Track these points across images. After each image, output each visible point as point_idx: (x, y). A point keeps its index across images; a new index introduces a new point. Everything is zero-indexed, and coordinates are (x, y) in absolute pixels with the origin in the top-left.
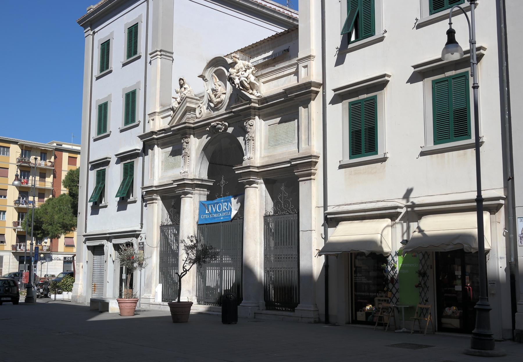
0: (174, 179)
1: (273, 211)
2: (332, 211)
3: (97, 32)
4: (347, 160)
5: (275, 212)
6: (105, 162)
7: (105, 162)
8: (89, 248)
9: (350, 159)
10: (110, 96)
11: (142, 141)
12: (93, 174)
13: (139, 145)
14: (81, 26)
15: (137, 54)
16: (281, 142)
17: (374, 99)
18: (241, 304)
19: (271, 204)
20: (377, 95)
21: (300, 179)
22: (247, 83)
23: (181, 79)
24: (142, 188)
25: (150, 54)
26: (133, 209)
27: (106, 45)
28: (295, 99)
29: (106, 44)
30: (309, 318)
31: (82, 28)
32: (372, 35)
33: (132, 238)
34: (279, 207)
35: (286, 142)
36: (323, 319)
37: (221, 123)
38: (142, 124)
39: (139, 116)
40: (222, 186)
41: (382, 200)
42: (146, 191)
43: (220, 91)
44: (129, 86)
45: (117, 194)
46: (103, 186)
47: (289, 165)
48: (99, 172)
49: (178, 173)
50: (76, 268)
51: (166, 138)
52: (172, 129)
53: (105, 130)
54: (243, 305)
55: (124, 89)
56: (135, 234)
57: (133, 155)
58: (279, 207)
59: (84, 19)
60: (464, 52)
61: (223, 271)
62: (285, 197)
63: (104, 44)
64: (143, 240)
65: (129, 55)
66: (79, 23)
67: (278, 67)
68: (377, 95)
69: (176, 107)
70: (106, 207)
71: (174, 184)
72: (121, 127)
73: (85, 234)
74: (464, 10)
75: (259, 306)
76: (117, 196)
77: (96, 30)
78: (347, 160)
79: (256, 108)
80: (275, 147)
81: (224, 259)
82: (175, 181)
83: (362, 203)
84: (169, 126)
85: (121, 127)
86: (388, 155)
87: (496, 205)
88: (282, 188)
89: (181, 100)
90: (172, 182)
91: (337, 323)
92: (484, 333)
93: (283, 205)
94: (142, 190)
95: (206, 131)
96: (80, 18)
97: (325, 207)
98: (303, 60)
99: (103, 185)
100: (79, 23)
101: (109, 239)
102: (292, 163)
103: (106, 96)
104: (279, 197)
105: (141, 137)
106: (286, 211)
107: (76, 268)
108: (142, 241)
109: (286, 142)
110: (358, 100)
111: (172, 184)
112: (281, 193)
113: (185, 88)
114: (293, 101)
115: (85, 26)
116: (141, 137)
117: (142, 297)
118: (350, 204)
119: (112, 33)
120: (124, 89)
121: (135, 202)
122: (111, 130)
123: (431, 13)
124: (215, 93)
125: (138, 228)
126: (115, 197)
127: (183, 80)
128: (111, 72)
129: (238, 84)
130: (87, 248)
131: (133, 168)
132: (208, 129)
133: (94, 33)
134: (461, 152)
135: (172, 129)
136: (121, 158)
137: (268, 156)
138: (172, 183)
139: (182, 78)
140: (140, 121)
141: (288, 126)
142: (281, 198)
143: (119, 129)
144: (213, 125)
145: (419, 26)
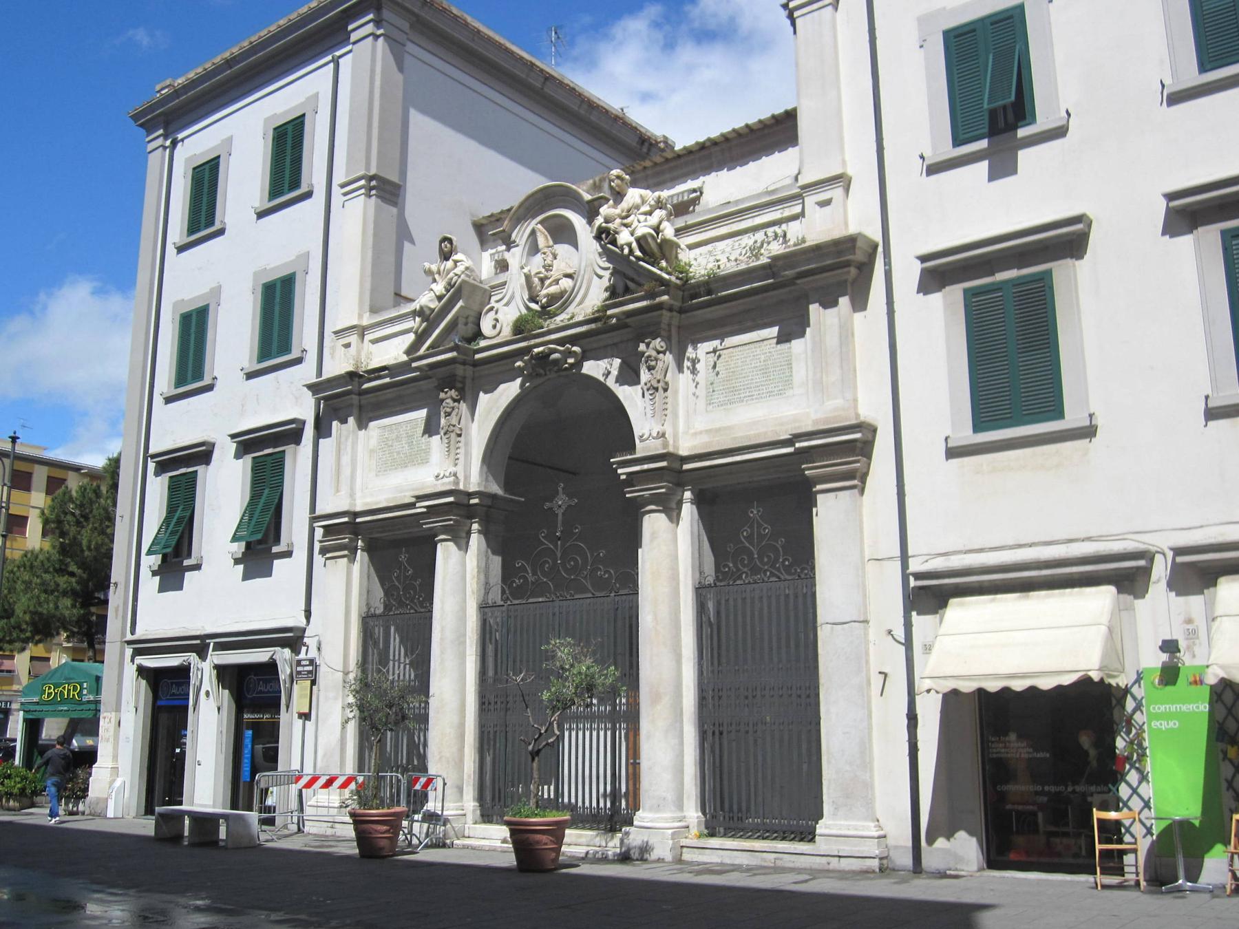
0: (421, 493)
1: (382, 606)
3: (182, 140)
4: (966, 435)
5: (387, 607)
6: (202, 454)
7: (202, 454)
8: (142, 671)
10: (217, 291)
12: (158, 488)
13: (305, 409)
14: (141, 126)
16: (748, 394)
19: (379, 593)
21: (819, 487)
23: (445, 239)
25: (343, 186)
26: (290, 572)
29: (207, 167)
31: (142, 131)
33: (189, 654)
34: (746, 562)
38: (311, 358)
39: (305, 334)
40: (560, 512)
41: (1083, 536)
42: (323, 527)
43: (557, 270)
44: (275, 262)
45: (236, 531)
46: (188, 514)
47: (790, 450)
51: (388, 391)
52: (414, 365)
53: (198, 374)
56: (292, 639)
57: (290, 434)
58: (746, 562)
59: (151, 109)
61: (567, 734)
62: (761, 537)
63: (202, 168)
64: (313, 653)
66: (135, 118)
69: (430, 309)
70: (197, 567)
71: (418, 505)
72: (247, 366)
73: (129, 637)
75: (688, 827)
76: (235, 539)
77: (180, 136)
78: (966, 435)
80: (729, 406)
82: (420, 498)
83: (1020, 546)
84: (405, 358)
86: (1099, 421)
87: (1134, 570)
88: (752, 512)
89: (448, 291)
90: (413, 500)
92: (224, 746)
93: (756, 556)
95: (514, 369)
96: (139, 105)
97: (904, 557)
99: (190, 511)
100: (135, 118)
101: (202, 652)
102: (797, 445)
104: (744, 537)
106: (768, 573)
108: (310, 656)
110: (993, 284)
111: (412, 505)
112: (751, 527)
113: (456, 262)
114: (793, 288)
115: (149, 127)
117: (308, 804)
118: (981, 550)
119: (230, 140)
120: (256, 275)
121: (288, 554)
122: (216, 374)
124: (542, 275)
125: (301, 622)
126: (231, 542)
127: (450, 241)
128: (221, 232)
129: (629, 245)
130: (1169, 688)
132: (519, 364)
133: (174, 143)
135: (414, 365)
136: (247, 443)
137: (708, 431)
139: (449, 236)
141: (770, 352)
142: (749, 538)
143: (242, 370)
144: (539, 353)
145: (1175, 99)
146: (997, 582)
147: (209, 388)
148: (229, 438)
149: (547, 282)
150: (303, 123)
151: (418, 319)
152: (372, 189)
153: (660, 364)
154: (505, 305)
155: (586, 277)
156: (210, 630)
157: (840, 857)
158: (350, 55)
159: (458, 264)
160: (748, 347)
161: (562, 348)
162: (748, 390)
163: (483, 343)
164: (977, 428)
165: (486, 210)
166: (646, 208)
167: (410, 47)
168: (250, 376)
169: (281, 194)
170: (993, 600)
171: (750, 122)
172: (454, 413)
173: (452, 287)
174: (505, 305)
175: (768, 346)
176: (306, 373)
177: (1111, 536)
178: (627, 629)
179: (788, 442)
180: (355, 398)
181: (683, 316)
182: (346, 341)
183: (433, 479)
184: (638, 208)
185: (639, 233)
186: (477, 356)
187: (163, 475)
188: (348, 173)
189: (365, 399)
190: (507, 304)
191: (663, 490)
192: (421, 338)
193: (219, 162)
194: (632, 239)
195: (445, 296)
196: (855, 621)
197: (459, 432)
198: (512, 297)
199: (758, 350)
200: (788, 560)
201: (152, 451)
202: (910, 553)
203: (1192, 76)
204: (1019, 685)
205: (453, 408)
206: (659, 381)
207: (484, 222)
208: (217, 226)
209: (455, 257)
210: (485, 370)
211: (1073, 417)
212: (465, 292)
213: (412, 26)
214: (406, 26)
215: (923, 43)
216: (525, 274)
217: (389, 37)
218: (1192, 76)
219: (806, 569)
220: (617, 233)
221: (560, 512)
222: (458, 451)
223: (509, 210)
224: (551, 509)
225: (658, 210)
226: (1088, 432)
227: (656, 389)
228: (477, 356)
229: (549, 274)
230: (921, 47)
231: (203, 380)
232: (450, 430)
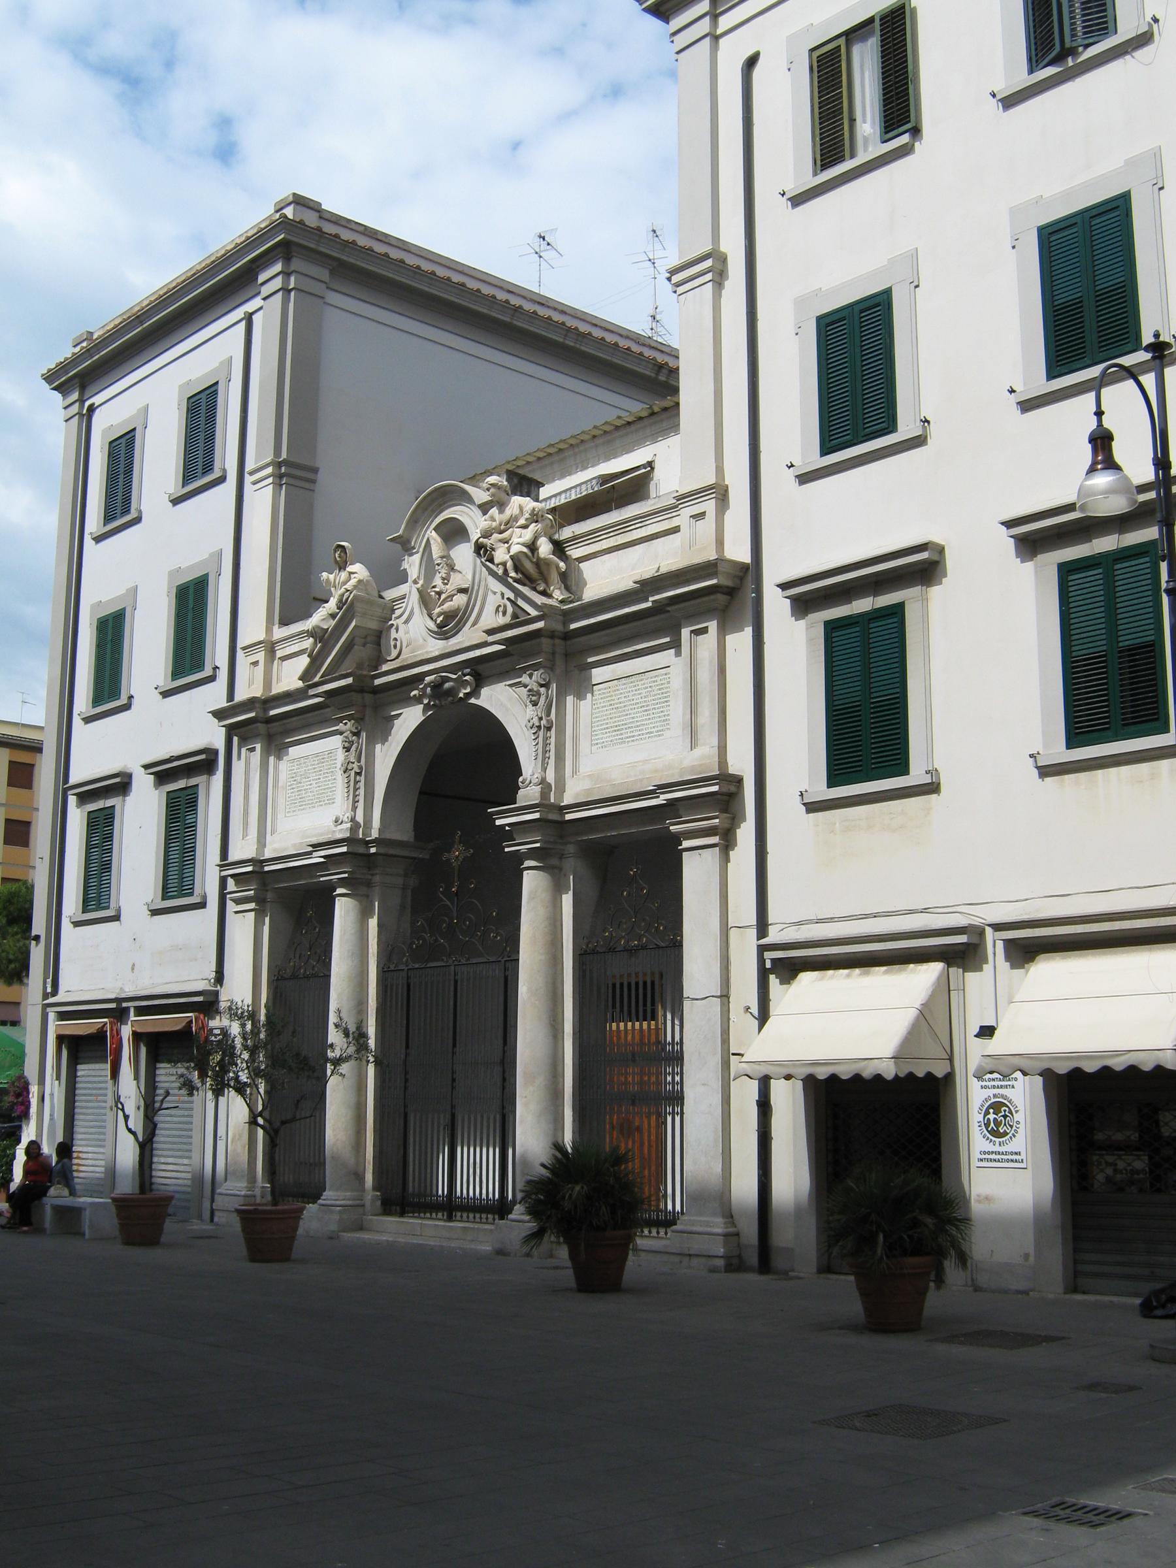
0: (315, 840)
2: (778, 939)
4: (1060, 752)
6: (121, 785)
7: (121, 785)
9: (828, 787)
11: (223, 726)
13: (214, 736)
15: (213, 472)
17: (897, 612)
18: (510, 1216)
20: (903, 603)
21: (686, 844)
22: (531, 561)
24: (220, 866)
27: (123, 445)
28: (668, 611)
29: (123, 440)
30: (709, 1256)
32: (888, 430)
35: (643, 734)
36: (753, 1259)
37: (454, 677)
38: (223, 675)
39: (217, 652)
48: (96, 815)
49: (329, 822)
50: (521, 1122)
53: (115, 693)
54: (324, 1202)
55: (173, 574)
60: (1137, 487)
63: (118, 442)
65: (188, 475)
67: (621, 516)
68: (903, 603)
71: (315, 854)
74: (1133, 370)
77: (97, 400)
79: (556, 633)
81: (669, 1078)
82: (317, 846)
84: (300, 684)
85: (161, 683)
89: (340, 608)
90: (310, 849)
91: (793, 1270)
94: (221, 871)
97: (762, 927)
98: (582, 537)
103: (122, 591)
105: (219, 714)
107: (521, 1122)
109: (643, 734)
113: (351, 573)
114: (663, 616)
116: (219, 714)
118: (831, 920)
120: (1013, 212)
123: (1051, 376)
128: (138, 520)
129: (504, 564)
131: (195, 806)
132: (415, 692)
134: (1144, 768)
136: (163, 773)
138: (310, 853)
140: (216, 668)
143: (156, 688)
146: (858, 955)
147: (127, 707)
148: (143, 769)
149: (443, 596)
150: (215, 393)
151: (311, 640)
152: (281, 476)
156: (130, 991)
157: (690, 1255)
158: (262, 311)
159: (352, 576)
161: (454, 677)
163: (385, 668)
164: (1071, 743)
166: (522, 521)
167: (334, 298)
168: (166, 694)
169: (114, 518)
170: (848, 976)
173: (344, 604)
176: (214, 695)
177: (853, 916)
178: (610, 991)
180: (261, 727)
182: (696, 510)
183: (332, 824)
184: (516, 519)
185: (515, 549)
186: (377, 682)
187: (1042, 558)
188: (256, 462)
189: (275, 727)
191: (538, 845)
192: (316, 660)
193: (216, 390)
194: (507, 557)
196: (713, 996)
198: (412, 613)
200: (662, 924)
201: (74, 779)
202: (771, 919)
203: (1041, 385)
204: (1118, 1064)
208: (133, 514)
209: (350, 568)
211: (917, 775)
212: (359, 607)
213: (332, 272)
214: (324, 274)
215: (1015, 243)
216: (418, 589)
217: (298, 289)
218: (1041, 385)
220: (493, 549)
224: (448, 860)
225: (534, 524)
226: (932, 788)
228: (377, 682)
230: (1014, 247)
231: (119, 698)
232: (349, 768)
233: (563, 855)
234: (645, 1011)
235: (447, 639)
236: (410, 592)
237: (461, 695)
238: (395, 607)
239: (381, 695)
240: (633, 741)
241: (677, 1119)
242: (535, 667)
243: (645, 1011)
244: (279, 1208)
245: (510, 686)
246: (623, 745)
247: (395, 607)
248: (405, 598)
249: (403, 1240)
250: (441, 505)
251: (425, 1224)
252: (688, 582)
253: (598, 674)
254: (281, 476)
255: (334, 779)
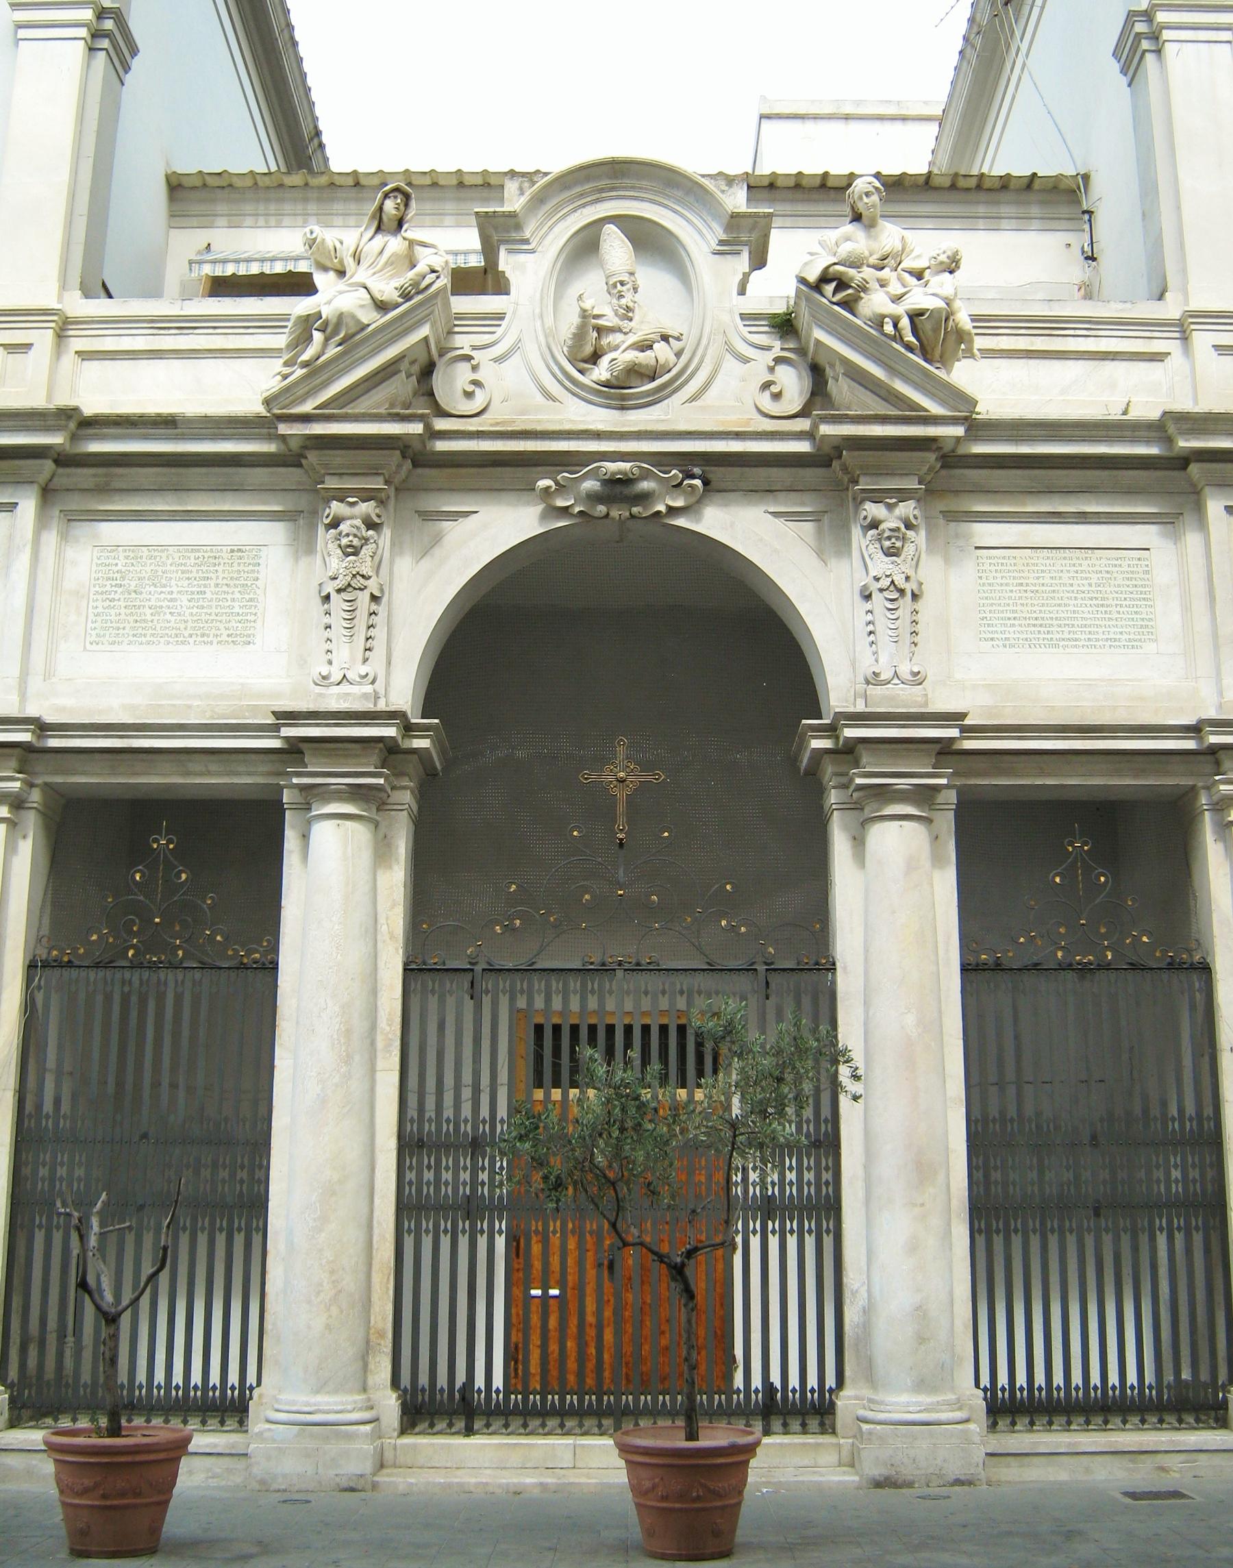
52: (283, 429)
69: (358, 321)
84: (261, 410)
89: (407, 297)
90: (271, 720)
141: (1108, 572)
153: (909, 549)
154: (496, 360)
155: (710, 352)
160: (1061, 553)
162: (1066, 629)
165: (187, 165)
171: (362, 169)
172: (366, 551)
173: (418, 293)
174: (496, 360)
175: (1104, 561)
179: (1195, 730)
181: (60, 470)
190: (499, 360)
195: (398, 305)
197: (377, 594)
199: (1085, 563)
205: (366, 540)
206: (907, 578)
207: (187, 182)
210: (84, 476)
219: (257, 951)
221: (621, 794)
222: (372, 632)
223: (546, 174)
227: (902, 592)
229: (625, 325)
233: (384, 804)
234: (556, 1067)
235: (622, 408)
236: (514, 313)
237: (661, 508)
238: (457, 329)
239: (426, 471)
240: (1075, 646)
241: (828, 1241)
242: (904, 495)
243: (556, 1067)
244: (702, 1443)
245: (775, 514)
246: (1054, 650)
247: (457, 329)
248: (502, 319)
249: (473, 1480)
250: (602, 190)
251: (583, 1446)
252: (1121, 439)
253: (985, 533)
254: (96, 34)
255: (251, 600)
